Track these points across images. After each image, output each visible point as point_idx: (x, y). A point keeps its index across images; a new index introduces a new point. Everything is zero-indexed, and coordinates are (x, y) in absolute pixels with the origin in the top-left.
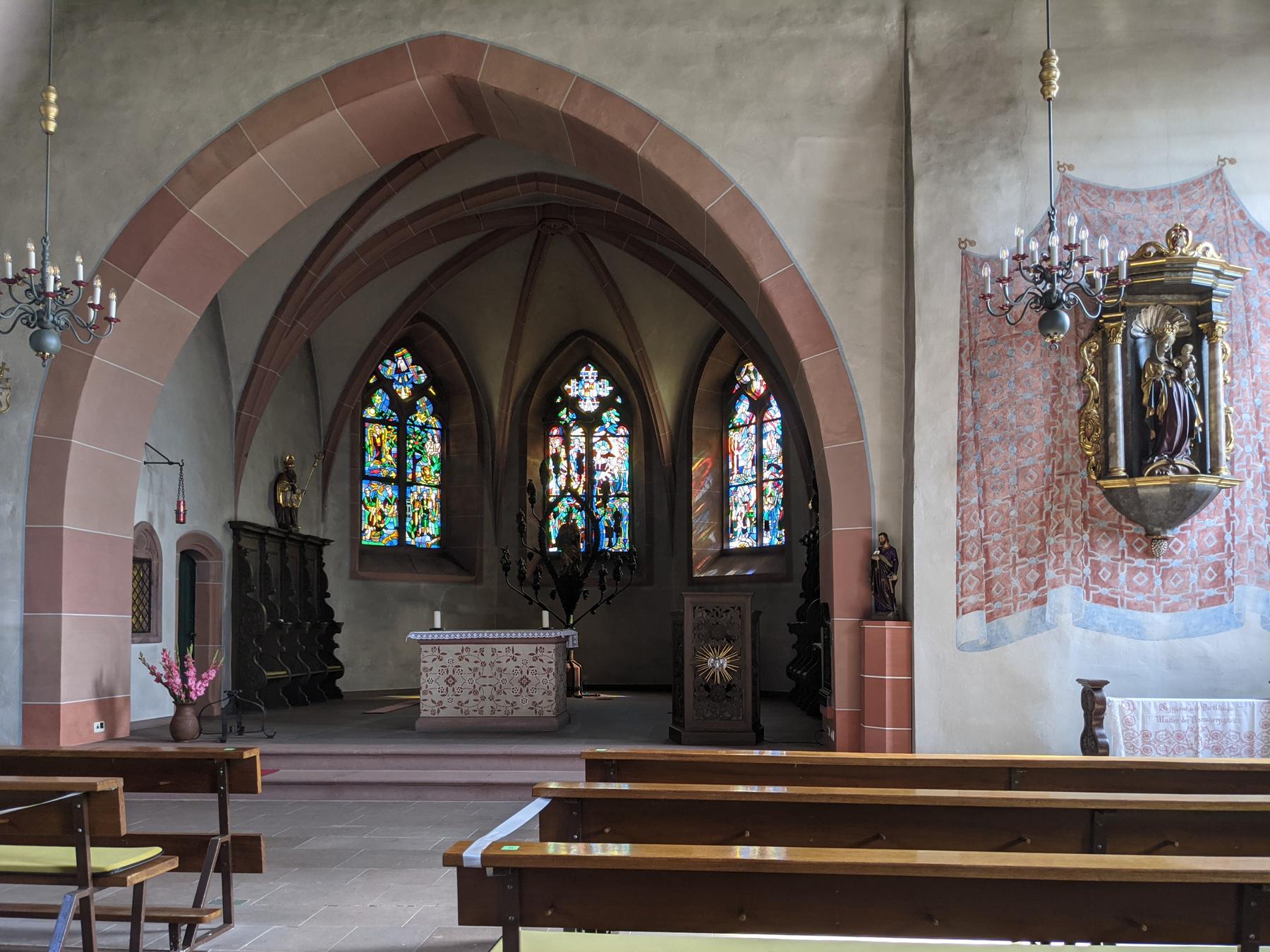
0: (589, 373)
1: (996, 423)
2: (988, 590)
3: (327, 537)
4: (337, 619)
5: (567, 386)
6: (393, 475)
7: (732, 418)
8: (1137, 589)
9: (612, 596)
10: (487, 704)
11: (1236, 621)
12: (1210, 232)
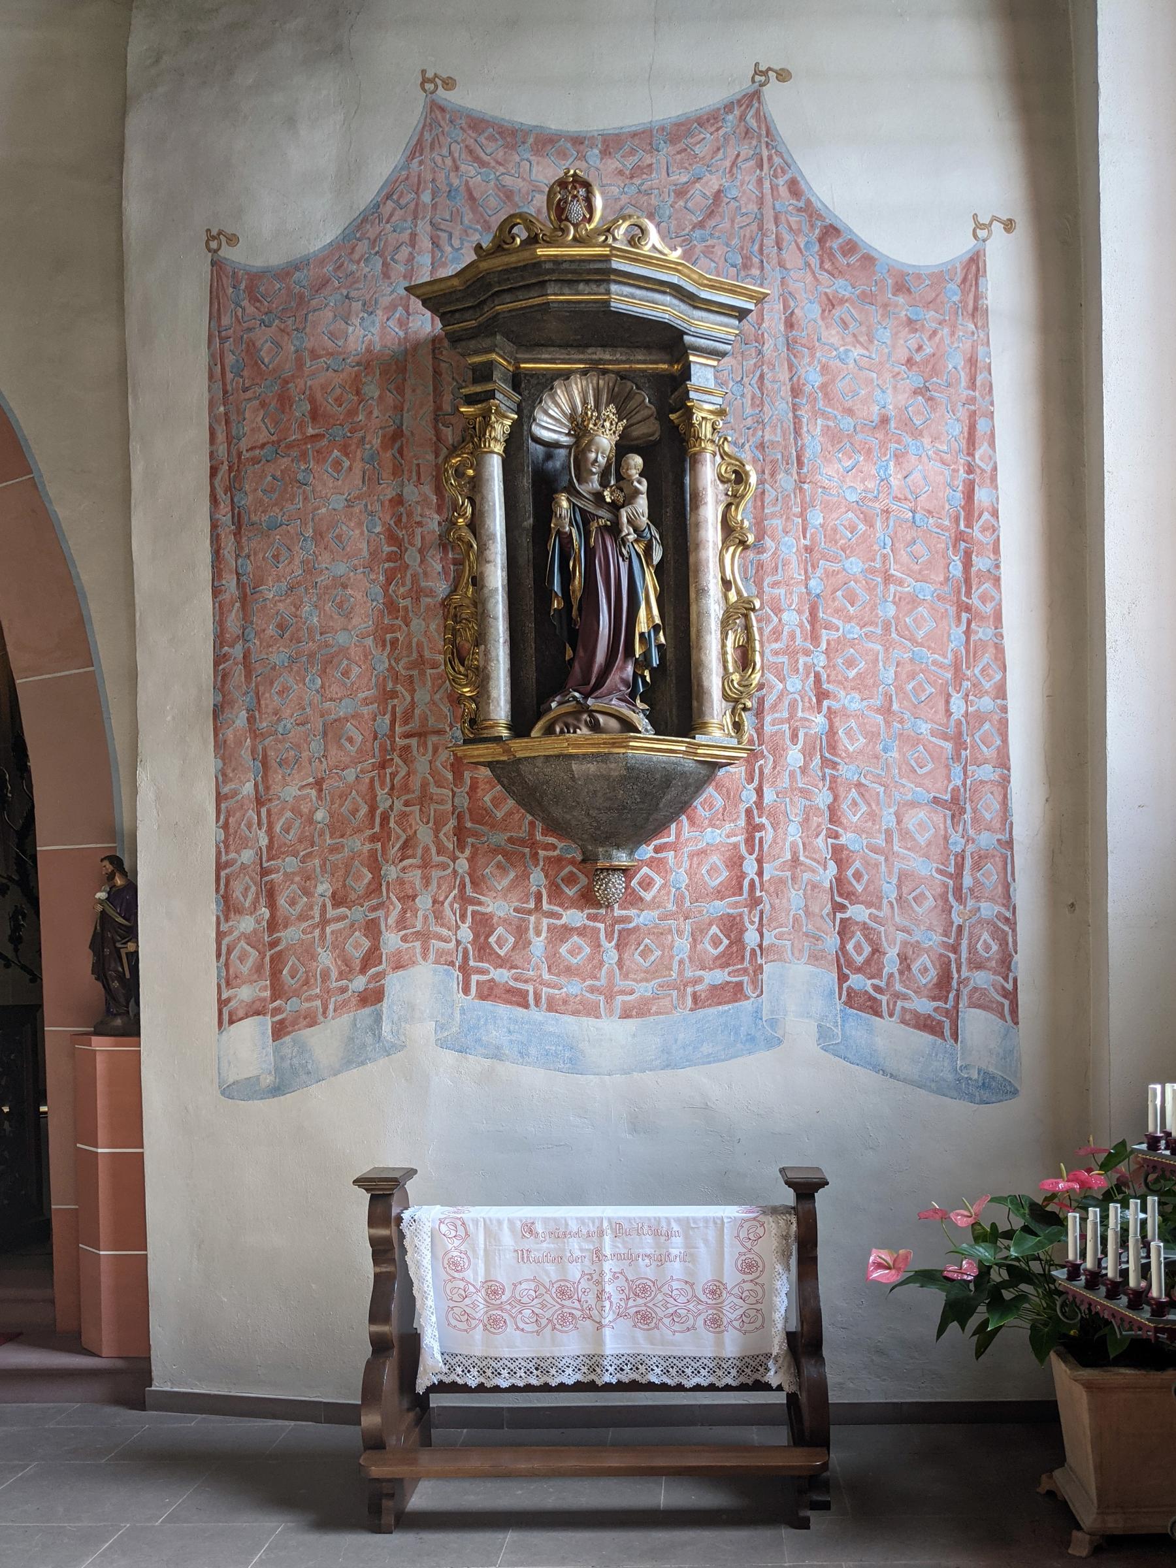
1: (282, 627)
2: (275, 974)
8: (569, 971)
11: (766, 1035)
12: (726, 224)
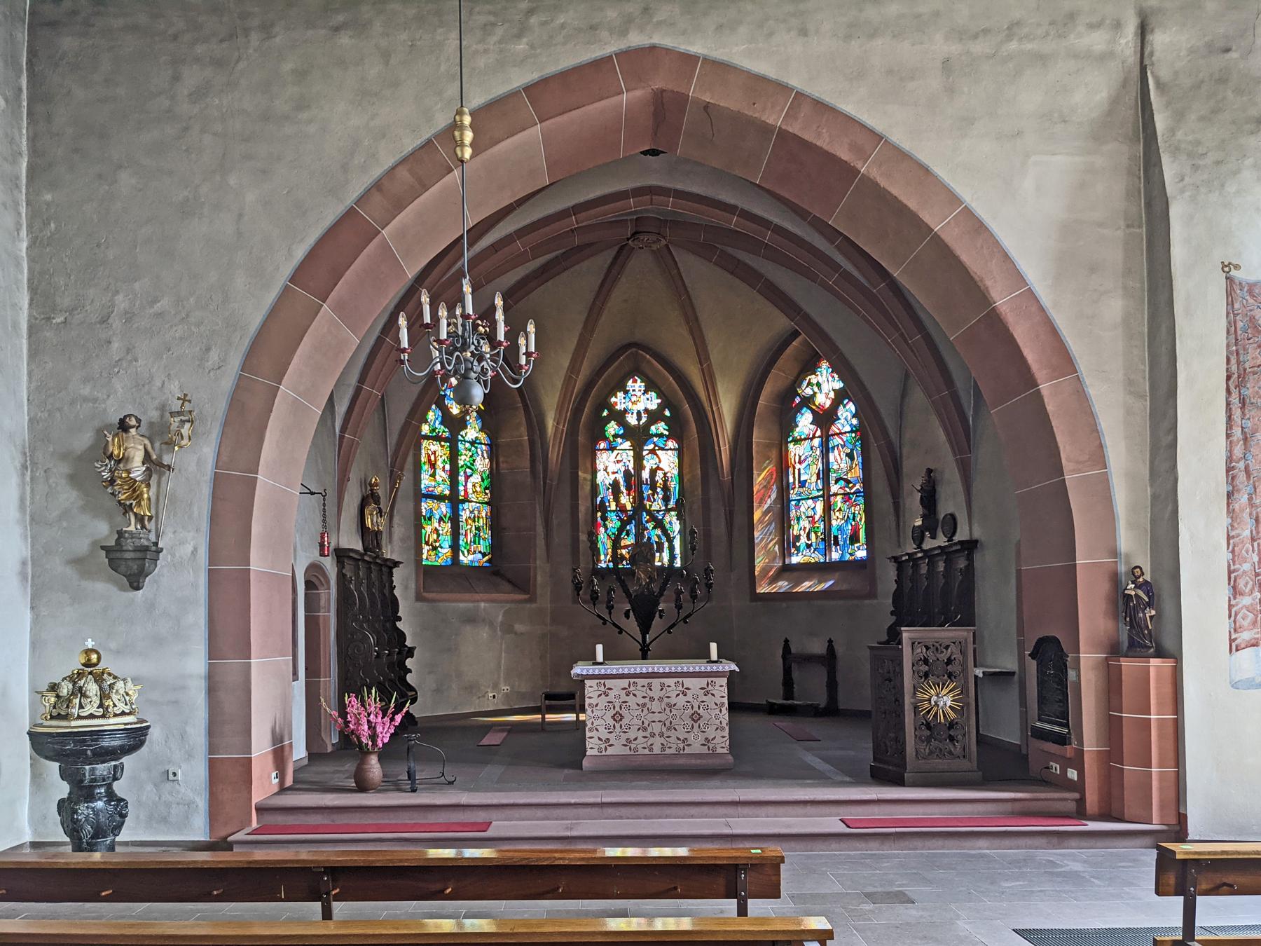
0: (636, 386)
3: (395, 557)
4: (408, 643)
5: (613, 400)
6: (447, 492)
7: (792, 430)
9: (689, 616)
10: (658, 741)
